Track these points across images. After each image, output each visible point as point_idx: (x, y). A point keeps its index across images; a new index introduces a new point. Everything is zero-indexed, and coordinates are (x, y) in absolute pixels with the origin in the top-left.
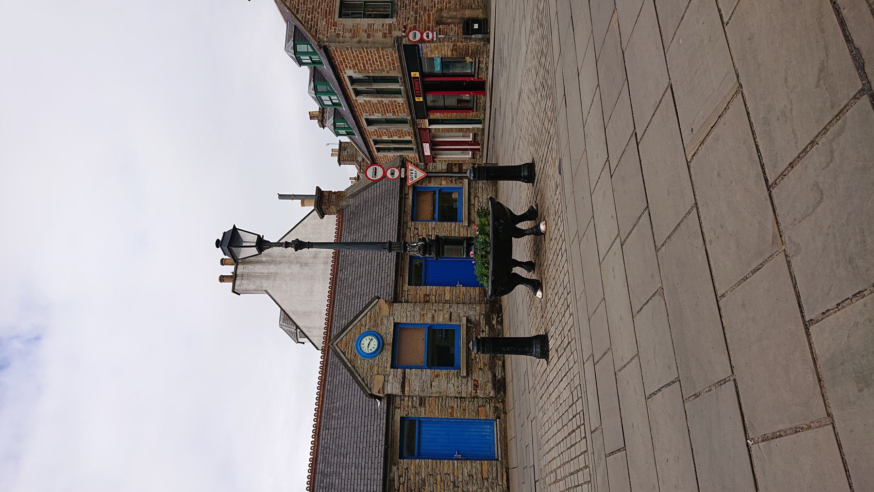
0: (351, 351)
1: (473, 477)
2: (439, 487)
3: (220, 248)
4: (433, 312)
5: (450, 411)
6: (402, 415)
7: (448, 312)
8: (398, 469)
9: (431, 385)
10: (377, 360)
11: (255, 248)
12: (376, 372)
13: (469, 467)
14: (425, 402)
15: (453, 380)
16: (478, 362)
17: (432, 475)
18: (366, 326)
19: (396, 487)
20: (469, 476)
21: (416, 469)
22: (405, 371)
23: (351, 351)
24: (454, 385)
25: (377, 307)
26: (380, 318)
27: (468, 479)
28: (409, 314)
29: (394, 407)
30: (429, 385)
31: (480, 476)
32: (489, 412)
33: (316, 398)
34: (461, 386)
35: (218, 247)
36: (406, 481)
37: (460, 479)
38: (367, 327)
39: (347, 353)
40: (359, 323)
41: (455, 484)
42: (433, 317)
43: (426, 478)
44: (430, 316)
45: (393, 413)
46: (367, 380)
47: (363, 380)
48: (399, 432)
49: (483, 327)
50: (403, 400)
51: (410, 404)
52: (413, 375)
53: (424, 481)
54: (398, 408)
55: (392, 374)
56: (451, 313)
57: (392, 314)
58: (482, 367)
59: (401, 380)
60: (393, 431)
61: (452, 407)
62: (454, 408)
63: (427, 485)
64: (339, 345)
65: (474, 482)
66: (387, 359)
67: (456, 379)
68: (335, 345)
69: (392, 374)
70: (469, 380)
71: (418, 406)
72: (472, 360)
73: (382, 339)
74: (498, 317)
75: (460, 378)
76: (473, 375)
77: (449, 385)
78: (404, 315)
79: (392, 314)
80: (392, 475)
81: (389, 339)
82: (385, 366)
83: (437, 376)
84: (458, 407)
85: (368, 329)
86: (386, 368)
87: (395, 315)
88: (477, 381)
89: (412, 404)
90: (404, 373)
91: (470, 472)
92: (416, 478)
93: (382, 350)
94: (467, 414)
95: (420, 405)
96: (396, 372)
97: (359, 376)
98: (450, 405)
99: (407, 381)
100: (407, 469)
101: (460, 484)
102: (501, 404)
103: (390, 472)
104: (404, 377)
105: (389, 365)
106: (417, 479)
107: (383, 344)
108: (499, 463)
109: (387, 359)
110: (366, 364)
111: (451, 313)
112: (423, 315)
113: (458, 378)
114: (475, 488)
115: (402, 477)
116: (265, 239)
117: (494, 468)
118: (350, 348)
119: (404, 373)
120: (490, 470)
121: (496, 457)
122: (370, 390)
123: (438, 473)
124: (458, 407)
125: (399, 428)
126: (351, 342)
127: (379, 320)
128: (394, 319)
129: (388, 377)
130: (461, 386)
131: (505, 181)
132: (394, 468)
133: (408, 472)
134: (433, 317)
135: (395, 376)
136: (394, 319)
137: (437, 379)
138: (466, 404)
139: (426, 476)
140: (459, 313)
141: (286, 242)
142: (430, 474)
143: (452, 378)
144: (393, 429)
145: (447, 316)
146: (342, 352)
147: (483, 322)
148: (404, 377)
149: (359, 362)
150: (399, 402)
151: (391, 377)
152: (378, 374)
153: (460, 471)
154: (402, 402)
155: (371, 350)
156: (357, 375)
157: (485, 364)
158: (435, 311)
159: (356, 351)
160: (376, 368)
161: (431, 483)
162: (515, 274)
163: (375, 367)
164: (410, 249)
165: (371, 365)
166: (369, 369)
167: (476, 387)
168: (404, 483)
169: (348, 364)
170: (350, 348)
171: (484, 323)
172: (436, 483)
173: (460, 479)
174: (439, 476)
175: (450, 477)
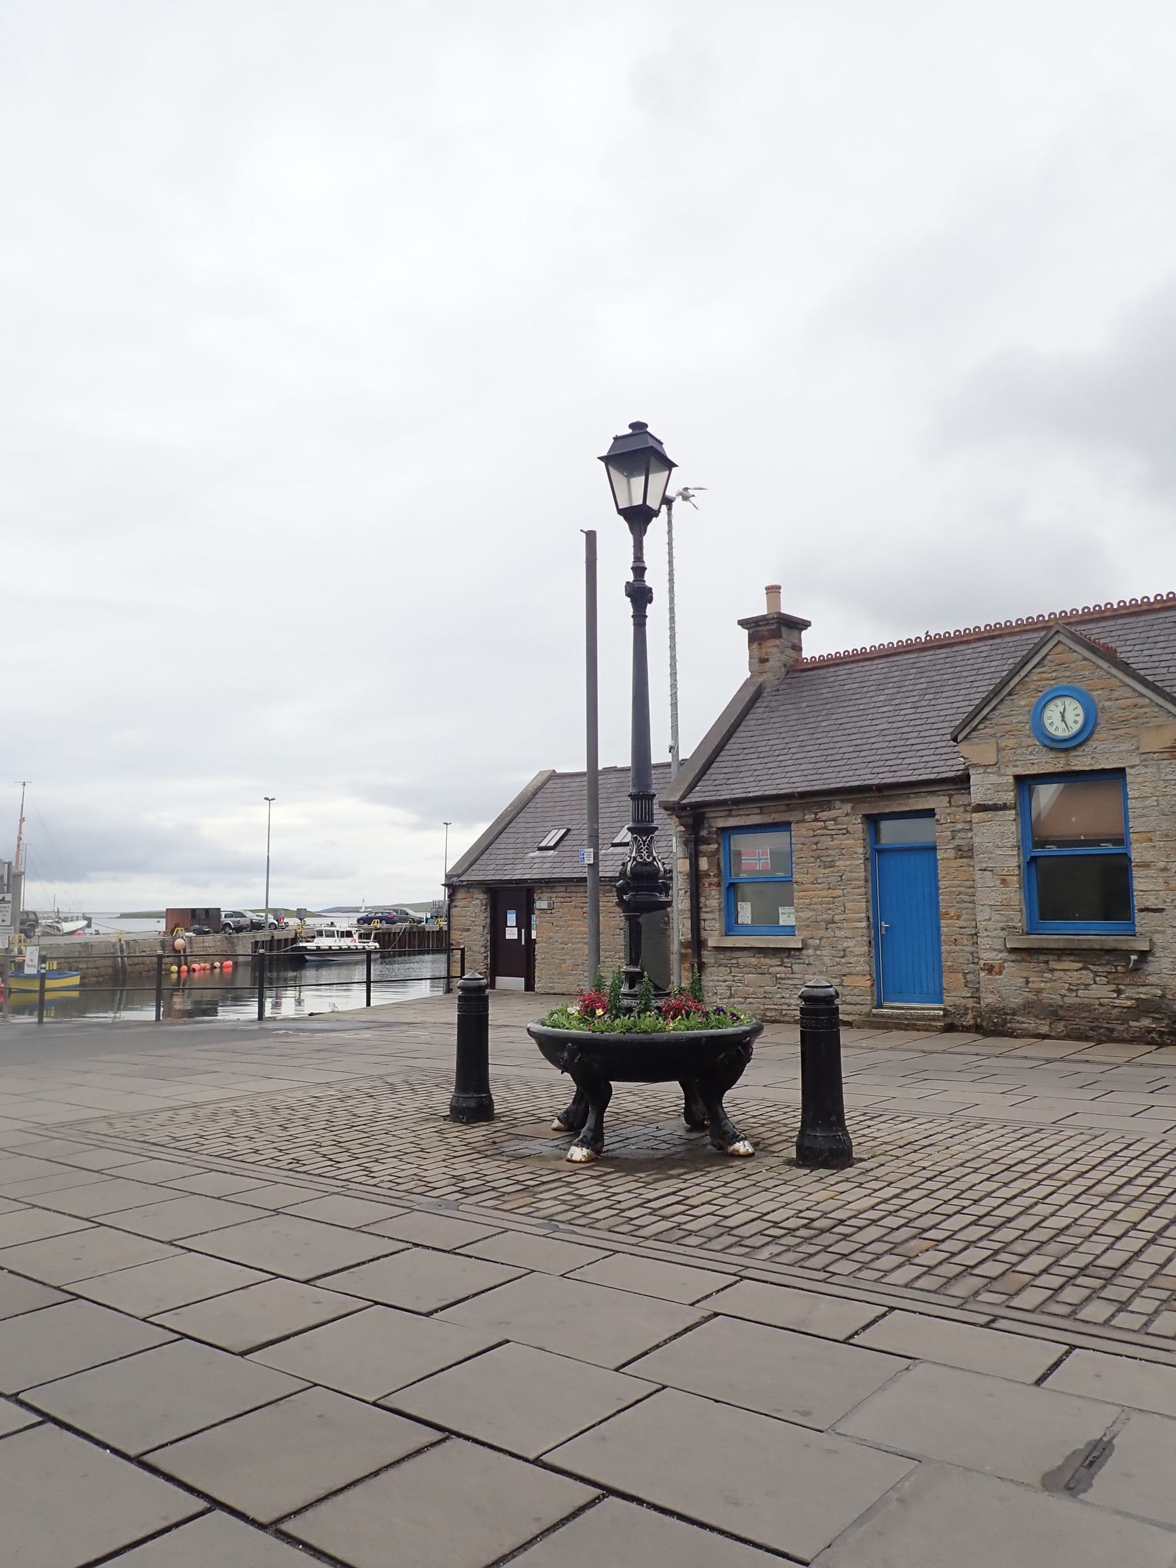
0: (1048, 679)
1: (843, 957)
2: (824, 893)
3: (630, 431)
4: (1162, 865)
5: (952, 912)
6: (937, 811)
7: (1165, 901)
8: (847, 815)
9: (985, 870)
10: (1030, 741)
11: (641, 503)
12: (1002, 745)
13: (858, 950)
14: (965, 857)
15: (998, 917)
16: (1042, 977)
17: (841, 880)
18: (1110, 699)
19: (820, 815)
20: (844, 951)
21: (848, 848)
22: (1010, 809)
23: (1048, 679)
24: (989, 920)
25: (1165, 719)
26: (1133, 731)
27: (840, 947)
28: (1151, 802)
29: (950, 792)
30: (984, 865)
31: (845, 970)
32: (955, 994)
33: (988, 625)
34: (987, 936)
35: (632, 426)
36: (829, 832)
37: (838, 933)
38: (1107, 704)
39: (1042, 669)
40: (1118, 683)
41: (831, 923)
42: (1146, 865)
43: (835, 869)
44: (1149, 857)
45: (940, 793)
46: (986, 727)
47: (985, 718)
48: (907, 809)
49: (1130, 992)
50: (965, 811)
51: (959, 826)
52: (1002, 829)
53: (831, 865)
54: (950, 802)
55: (1003, 780)
56: (1161, 910)
57: (1146, 760)
58: (1030, 985)
59: (990, 803)
60: (908, 796)
61: (959, 917)
62: (958, 919)
63: (827, 871)
64: (1060, 648)
65: (837, 959)
66: (1033, 764)
67: (1002, 925)
68: (1057, 638)
69: (1003, 780)
70: (1001, 955)
71: (957, 842)
72: (1047, 962)
73: (1080, 745)
74: (1161, 1034)
75: (1002, 934)
76: (1012, 964)
77: (988, 909)
78: (1148, 791)
79: (1146, 760)
80: (838, 804)
81: (1081, 762)
82: (1018, 763)
83: (1003, 881)
84: (961, 928)
85: (1104, 708)
86: (1015, 766)
87: (1146, 766)
88: (1000, 973)
89: (959, 831)
90: (1005, 807)
91: (851, 952)
92: (834, 849)
93: (1052, 749)
94: (948, 948)
95: (958, 848)
96: (1005, 788)
97: (994, 709)
98: (964, 912)
99: (990, 814)
100: (848, 832)
101: (830, 933)
102: (972, 1022)
103: (842, 801)
104: (995, 808)
105: (1020, 771)
106: (833, 853)
107: (1066, 750)
108: (868, 1010)
109: (1033, 764)
110: (1020, 718)
111: (1161, 910)
112: (1151, 840)
113: (1003, 929)
114: (827, 960)
115: (836, 824)
116: (654, 519)
117: (858, 999)
118: (1054, 674)
119: (1005, 807)
120: (856, 991)
121: (886, 1004)
122: (965, 738)
123: (845, 891)
124: (961, 928)
125: (914, 808)
126: (1068, 674)
127: (1127, 730)
128: (1132, 767)
129: (994, 773)
130: (987, 936)
131: (800, 1092)
132: (848, 807)
133: (844, 834)
134: (1146, 865)
135: (997, 788)
136: (1132, 767)
137: (998, 883)
138: (966, 945)
139: (839, 869)
140: (1163, 932)
141: (646, 568)
142: (841, 876)
143: (1002, 915)
144: (912, 795)
145: (1151, 902)
146: (1043, 658)
147: (1143, 993)
148: (995, 808)
149: (1023, 703)
150: (961, 803)
151: (994, 778)
152: (999, 750)
153: (849, 933)
154: (962, 809)
155: (1076, 722)
156: (993, 704)
157: (1039, 991)
158: (1165, 869)
159: (1048, 689)
160: (1011, 742)
161: (830, 879)
162: (610, 1085)
163: (1015, 741)
164: (644, 842)
165: (1018, 731)
166: (1008, 728)
167: (988, 970)
168: (825, 828)
169: (1017, 679)
170: (1054, 674)
171: (1142, 996)
172: (829, 888)
173: (838, 933)
174: (840, 892)
175: (840, 914)
